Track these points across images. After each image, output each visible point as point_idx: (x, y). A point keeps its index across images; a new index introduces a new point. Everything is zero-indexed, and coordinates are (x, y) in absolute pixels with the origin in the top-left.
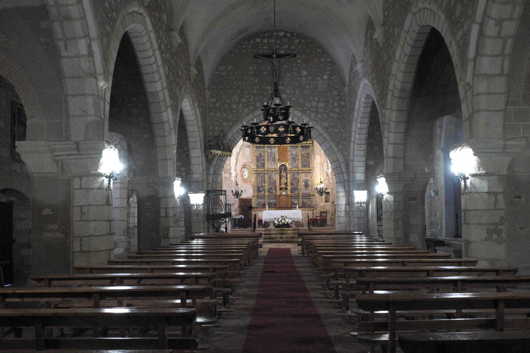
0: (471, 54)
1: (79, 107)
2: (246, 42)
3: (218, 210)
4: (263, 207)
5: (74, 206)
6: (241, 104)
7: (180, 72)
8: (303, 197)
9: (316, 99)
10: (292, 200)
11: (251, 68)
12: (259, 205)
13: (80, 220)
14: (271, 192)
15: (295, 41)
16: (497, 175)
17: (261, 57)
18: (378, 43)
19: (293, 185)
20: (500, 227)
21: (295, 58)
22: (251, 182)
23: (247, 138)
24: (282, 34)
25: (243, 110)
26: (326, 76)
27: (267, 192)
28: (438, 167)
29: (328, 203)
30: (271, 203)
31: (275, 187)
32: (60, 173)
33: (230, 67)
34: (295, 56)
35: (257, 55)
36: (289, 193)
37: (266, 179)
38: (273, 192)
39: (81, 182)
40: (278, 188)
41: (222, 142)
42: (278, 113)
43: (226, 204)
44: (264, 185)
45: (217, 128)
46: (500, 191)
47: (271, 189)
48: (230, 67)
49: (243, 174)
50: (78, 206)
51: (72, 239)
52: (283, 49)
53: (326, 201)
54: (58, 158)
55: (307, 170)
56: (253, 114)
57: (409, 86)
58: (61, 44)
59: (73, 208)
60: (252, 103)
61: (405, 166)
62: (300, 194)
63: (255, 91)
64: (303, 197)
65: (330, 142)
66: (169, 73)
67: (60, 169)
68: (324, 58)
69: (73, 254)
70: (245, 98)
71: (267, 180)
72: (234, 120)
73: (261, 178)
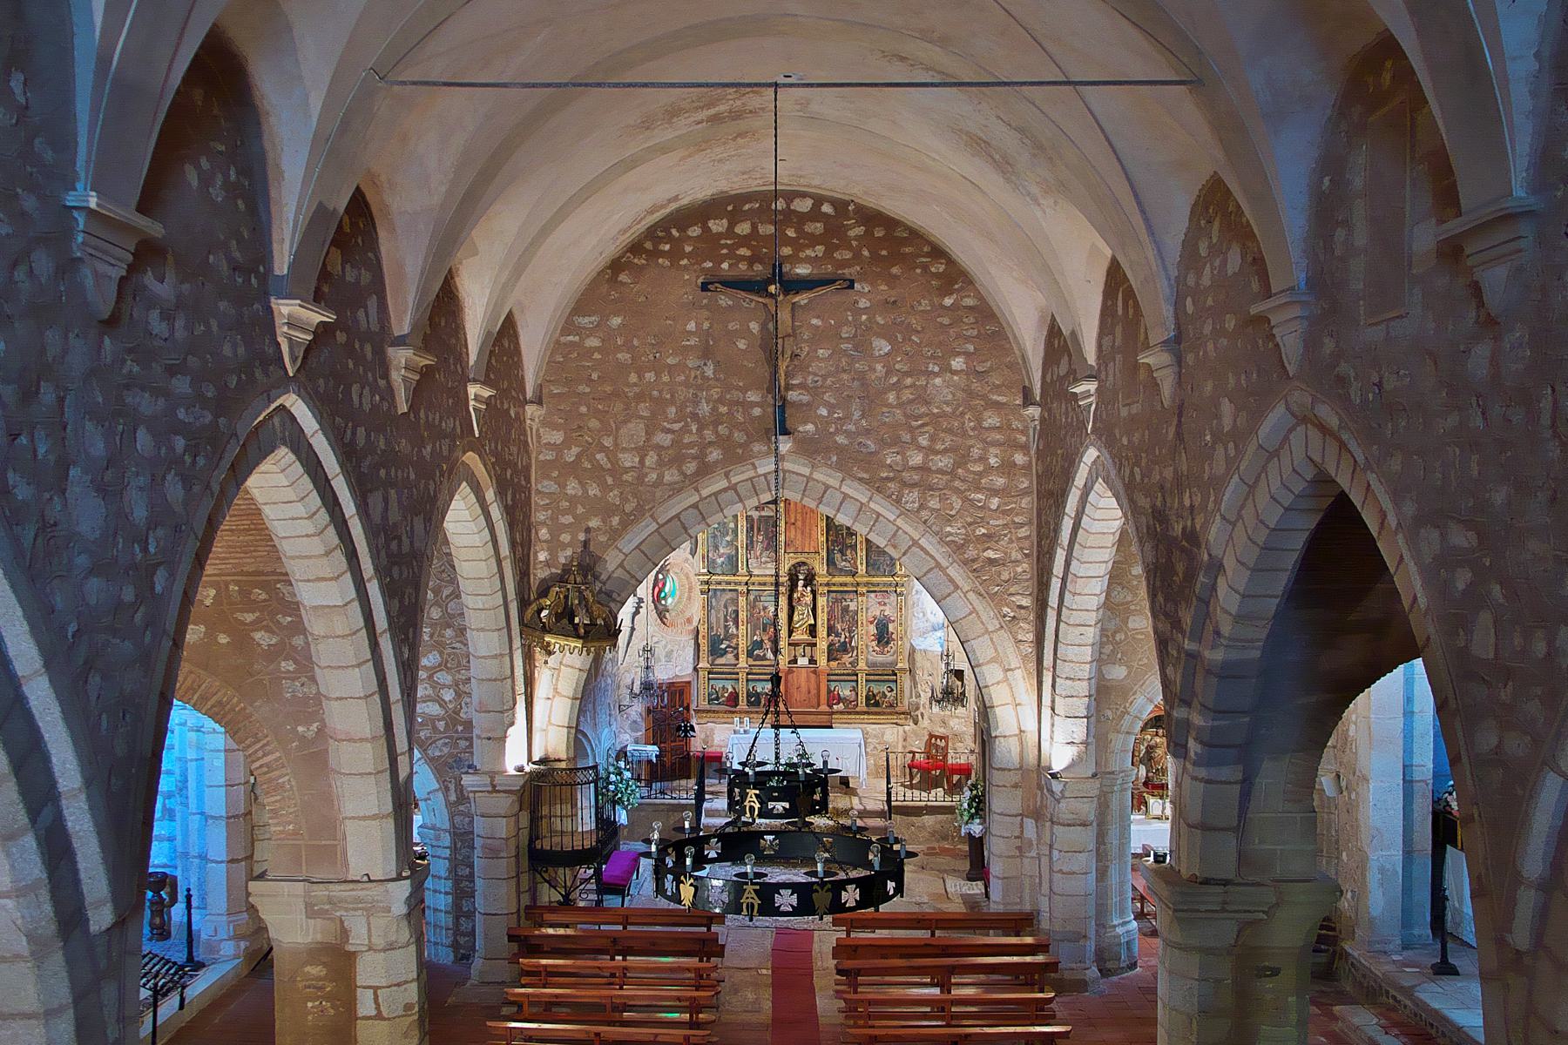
2: (675, 232)
3: (570, 819)
6: (651, 453)
8: (872, 678)
9: (923, 441)
10: (833, 685)
11: (691, 326)
12: (717, 699)
14: (758, 655)
15: (852, 233)
19: (838, 635)
21: (850, 291)
22: (689, 621)
24: (803, 206)
25: (661, 476)
26: (960, 359)
27: (743, 657)
30: (758, 695)
33: (616, 321)
34: (851, 287)
35: (712, 283)
36: (822, 661)
37: (740, 614)
38: (764, 658)
40: (783, 644)
44: (733, 630)
45: (565, 538)
47: (759, 644)
48: (616, 321)
49: (660, 592)
52: (808, 260)
55: (885, 585)
56: (697, 490)
60: (693, 451)
61: (1242, 858)
62: (862, 665)
63: (705, 409)
64: (872, 678)
65: (971, 596)
68: (955, 296)
70: (669, 431)
71: (742, 616)
72: (628, 508)
73: (726, 607)
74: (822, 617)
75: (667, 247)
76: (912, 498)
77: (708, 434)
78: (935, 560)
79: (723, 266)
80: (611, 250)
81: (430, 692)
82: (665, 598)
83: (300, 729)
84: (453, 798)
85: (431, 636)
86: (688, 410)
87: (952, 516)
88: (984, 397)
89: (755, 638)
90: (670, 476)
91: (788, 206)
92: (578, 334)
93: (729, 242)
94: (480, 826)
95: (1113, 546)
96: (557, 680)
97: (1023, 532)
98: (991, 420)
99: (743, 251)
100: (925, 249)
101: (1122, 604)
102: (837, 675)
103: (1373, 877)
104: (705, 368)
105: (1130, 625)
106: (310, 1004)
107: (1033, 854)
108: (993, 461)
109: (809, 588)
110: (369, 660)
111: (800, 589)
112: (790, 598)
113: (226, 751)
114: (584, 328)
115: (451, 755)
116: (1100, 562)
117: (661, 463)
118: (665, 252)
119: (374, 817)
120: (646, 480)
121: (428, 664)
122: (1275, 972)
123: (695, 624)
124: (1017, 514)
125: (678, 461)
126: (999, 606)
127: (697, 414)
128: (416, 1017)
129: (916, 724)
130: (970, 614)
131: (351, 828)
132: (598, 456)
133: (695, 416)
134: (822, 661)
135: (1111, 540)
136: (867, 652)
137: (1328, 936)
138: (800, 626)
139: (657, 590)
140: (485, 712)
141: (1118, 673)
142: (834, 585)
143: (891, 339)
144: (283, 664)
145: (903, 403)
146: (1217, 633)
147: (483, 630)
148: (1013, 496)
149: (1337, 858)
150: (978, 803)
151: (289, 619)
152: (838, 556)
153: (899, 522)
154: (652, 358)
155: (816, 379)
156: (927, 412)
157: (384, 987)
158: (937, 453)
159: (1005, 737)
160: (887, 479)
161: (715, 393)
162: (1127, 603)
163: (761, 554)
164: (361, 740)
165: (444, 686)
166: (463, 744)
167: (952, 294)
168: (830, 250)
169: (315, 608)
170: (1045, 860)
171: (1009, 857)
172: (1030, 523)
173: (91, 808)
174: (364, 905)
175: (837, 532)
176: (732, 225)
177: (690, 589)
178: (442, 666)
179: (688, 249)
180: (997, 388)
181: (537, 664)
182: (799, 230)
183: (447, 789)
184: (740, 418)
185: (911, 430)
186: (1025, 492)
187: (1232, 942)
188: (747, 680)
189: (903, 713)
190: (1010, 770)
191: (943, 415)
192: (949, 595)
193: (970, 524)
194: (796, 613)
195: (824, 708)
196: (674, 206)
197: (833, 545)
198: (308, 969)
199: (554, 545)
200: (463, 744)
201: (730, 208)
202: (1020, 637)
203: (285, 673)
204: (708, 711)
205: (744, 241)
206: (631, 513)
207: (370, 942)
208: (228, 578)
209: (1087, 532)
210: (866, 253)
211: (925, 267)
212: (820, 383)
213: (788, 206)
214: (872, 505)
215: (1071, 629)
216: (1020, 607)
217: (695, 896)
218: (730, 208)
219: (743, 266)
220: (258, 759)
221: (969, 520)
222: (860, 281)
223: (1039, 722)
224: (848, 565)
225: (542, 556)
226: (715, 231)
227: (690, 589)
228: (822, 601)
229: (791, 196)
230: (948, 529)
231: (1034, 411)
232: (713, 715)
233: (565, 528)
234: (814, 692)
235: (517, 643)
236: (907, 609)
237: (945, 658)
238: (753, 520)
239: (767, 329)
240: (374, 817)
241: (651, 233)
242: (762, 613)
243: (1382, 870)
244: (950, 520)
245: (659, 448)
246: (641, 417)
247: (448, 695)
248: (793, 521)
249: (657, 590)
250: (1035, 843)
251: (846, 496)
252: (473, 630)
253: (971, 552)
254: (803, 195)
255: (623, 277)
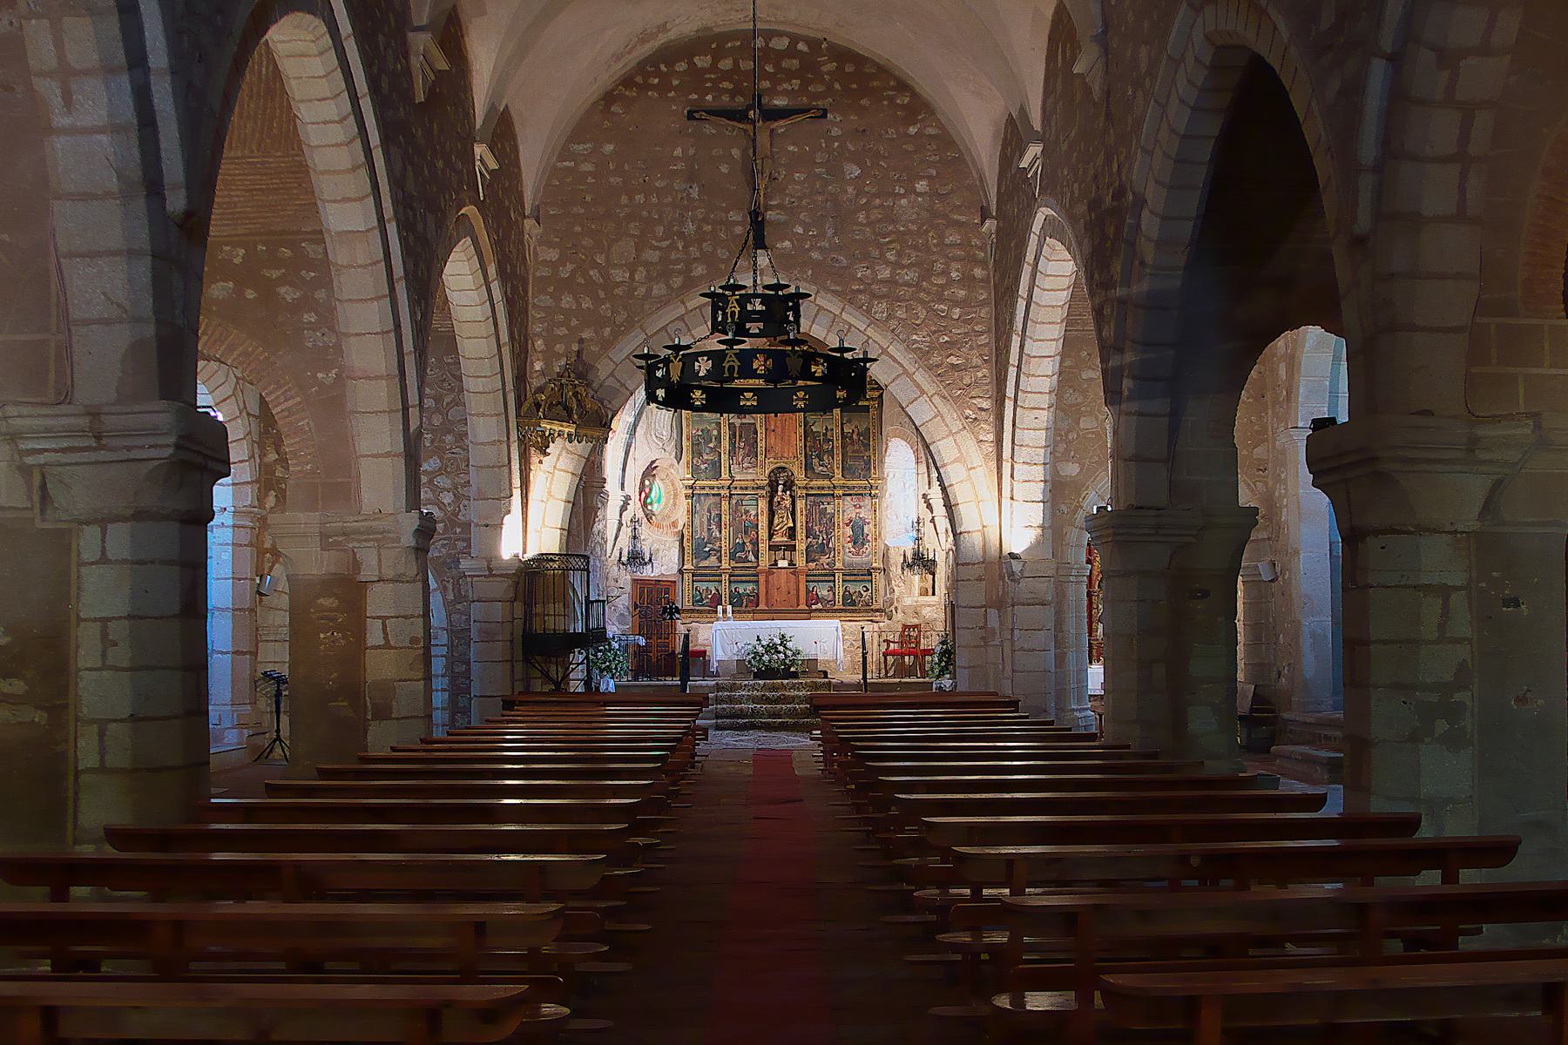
0: (1368, 150)
1: (104, 294)
4: (708, 607)
5: (79, 620)
7: (440, 164)
8: (848, 578)
10: (811, 585)
11: (678, 152)
13: (99, 665)
15: (824, 69)
16: (1449, 533)
17: (712, 118)
18: (1088, 90)
20: (1457, 697)
22: (674, 524)
23: (661, 393)
24: (781, 44)
25: (649, 290)
28: (1283, 487)
29: (930, 599)
31: (755, 543)
32: (37, 511)
34: (824, 116)
35: (697, 112)
36: (800, 561)
37: (723, 516)
38: (746, 560)
39: (103, 541)
40: (763, 546)
41: (576, 394)
42: (731, 368)
43: (589, 602)
46: (1459, 584)
49: (647, 497)
50: (95, 620)
51: (72, 728)
52: (785, 93)
53: (924, 592)
54: (29, 460)
56: (683, 303)
57: (1187, 229)
58: (49, 89)
59: (78, 626)
62: (838, 565)
63: (691, 228)
64: (848, 578)
65: (936, 399)
66: (405, 169)
67: (36, 498)
69: (76, 778)
70: (656, 248)
71: (725, 519)
72: (619, 320)
73: (709, 511)
74: (801, 520)
75: (656, 81)
76: (880, 308)
78: (902, 366)
79: (707, 98)
80: (606, 78)
81: (430, 495)
82: (651, 504)
83: (320, 375)
84: (451, 597)
85: (432, 442)
86: (675, 228)
87: (917, 325)
88: (945, 216)
89: (737, 541)
90: (658, 289)
91: (767, 45)
92: (573, 160)
93: (713, 76)
94: (476, 611)
95: (1062, 321)
96: (551, 483)
97: (983, 339)
98: (953, 237)
99: (726, 85)
100: (892, 84)
101: (1074, 405)
102: (815, 575)
103: (1306, 643)
104: (691, 191)
105: (1082, 426)
107: (997, 642)
108: (954, 275)
109: (788, 492)
110: (385, 296)
111: (780, 493)
112: (771, 503)
113: (233, 544)
114: (579, 154)
115: (449, 555)
116: (1051, 340)
117: (649, 278)
118: (653, 85)
119: (388, 455)
121: (430, 469)
122: (1206, 594)
123: (680, 528)
124: (977, 323)
125: (665, 275)
126: (961, 408)
127: (684, 232)
128: (421, 652)
130: (935, 417)
131: (364, 464)
133: (681, 235)
134: (800, 561)
135: (1060, 314)
136: (845, 555)
137: (1269, 717)
138: (781, 529)
139: (643, 495)
140: (484, 499)
141: (1071, 470)
142: (812, 488)
143: (861, 164)
145: (872, 223)
146: (1142, 263)
147: (483, 415)
148: (972, 307)
149: (1275, 644)
150: (949, 658)
151: (313, 274)
152: (816, 461)
153: (870, 332)
154: (641, 181)
155: (792, 200)
156: (894, 230)
157: (392, 617)
158: (903, 267)
159: (969, 532)
160: (858, 290)
161: (700, 213)
162: (1079, 404)
163: (743, 460)
164: (376, 378)
166: (461, 545)
167: (915, 124)
168: (805, 84)
169: (339, 234)
170: (1007, 644)
171: (975, 647)
172: (989, 331)
173: (174, 92)
174: (375, 536)
175: (815, 438)
176: (716, 60)
177: (675, 495)
178: (442, 471)
179: (675, 82)
180: (957, 209)
181: (532, 468)
182: (777, 66)
183: (445, 588)
185: (880, 246)
186: (983, 303)
188: (730, 582)
189: (877, 611)
190: (974, 564)
191: (909, 232)
192: (916, 399)
193: (934, 333)
195: (803, 607)
196: (662, 39)
197: (810, 450)
198: (321, 601)
199: (549, 355)
200: (461, 545)
201: (713, 46)
202: (981, 437)
203: (307, 323)
204: (692, 611)
205: (726, 76)
206: (622, 325)
207: (380, 572)
208: (257, 238)
209: (1040, 306)
210: (837, 86)
211: (891, 99)
212: (796, 204)
213: (767, 45)
214: (844, 316)
215: (1027, 412)
216: (981, 409)
217: (682, 372)
218: (713, 46)
219: (726, 98)
220: (280, 404)
221: (933, 328)
222: (832, 113)
223: (1000, 516)
224: (825, 469)
225: (538, 366)
226: (700, 66)
227: (675, 495)
228: (800, 504)
229: (769, 35)
230: (915, 337)
231: (990, 225)
232: (697, 615)
233: (559, 339)
234: (793, 592)
235: (514, 436)
236: (881, 512)
237: (916, 524)
238: (735, 427)
239: (748, 155)
240: (388, 455)
241: (641, 67)
242: (744, 517)
243: (1313, 635)
244: (916, 328)
245: (647, 264)
247: (447, 498)
248: (773, 428)
249: (643, 495)
250: (998, 632)
251: (820, 308)
252: (473, 415)
253: (936, 359)
254: (780, 34)
255: (615, 108)
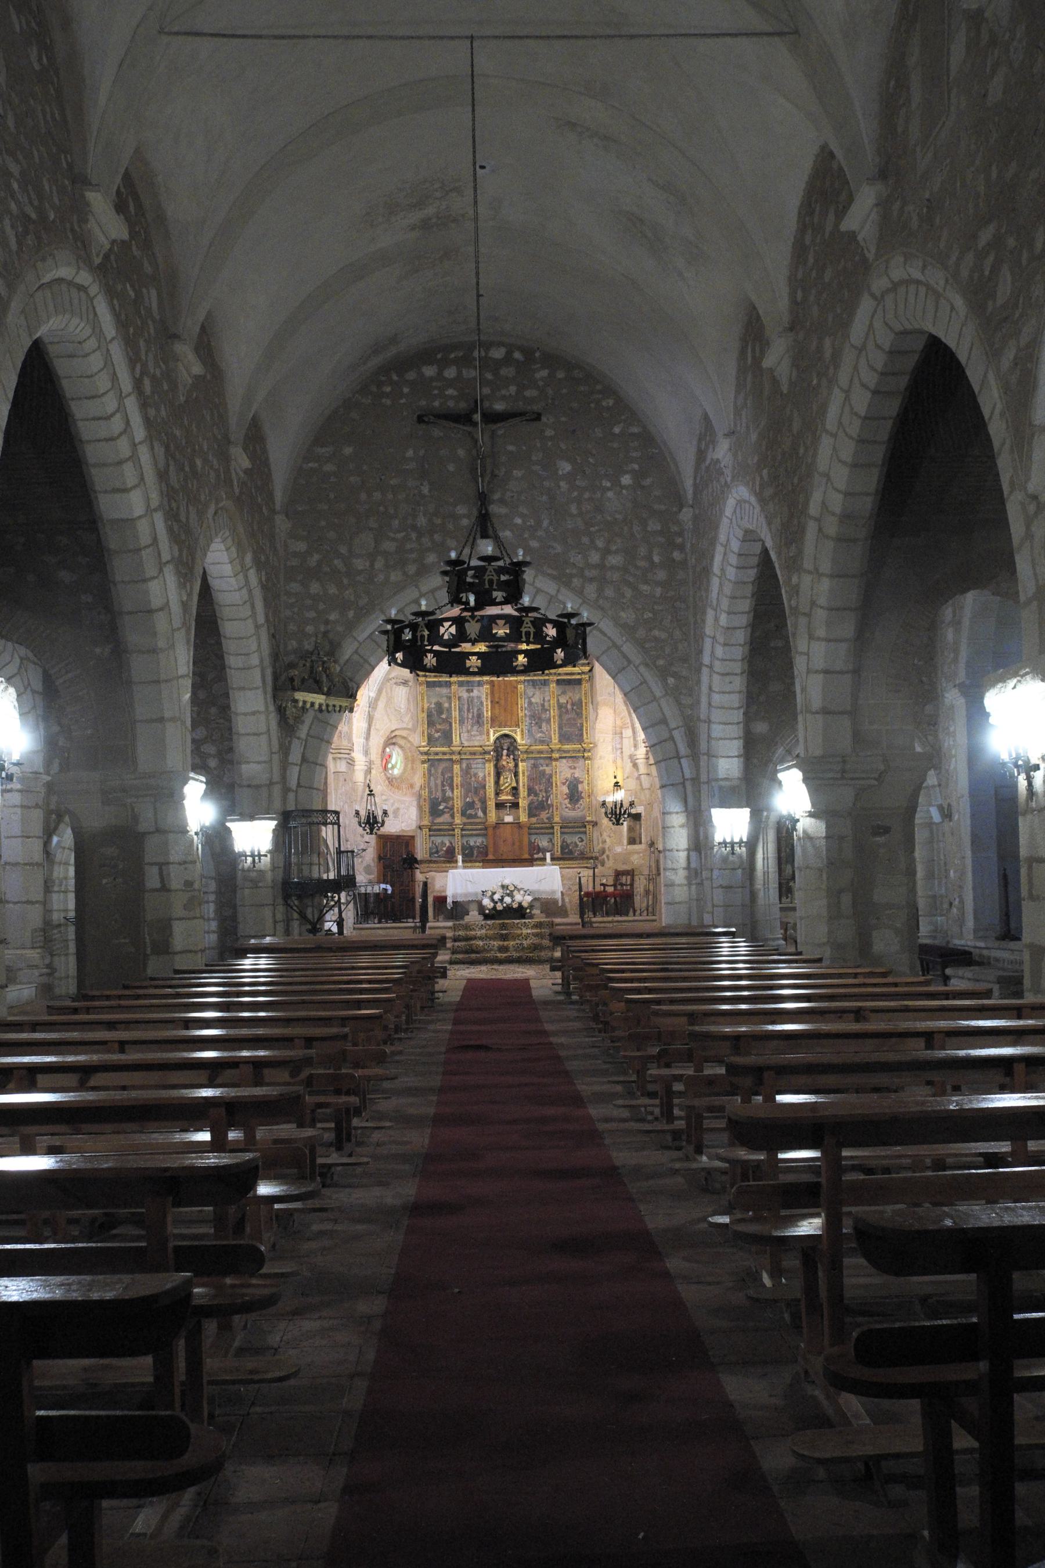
9: (600, 544)
11: (410, 453)
12: (437, 852)
15: (538, 375)
19: (536, 795)
24: (498, 354)
30: (471, 848)
35: (426, 415)
38: (476, 816)
44: (449, 793)
48: (348, 451)
49: (387, 762)
52: (504, 398)
55: (574, 751)
62: (557, 819)
64: (566, 830)
70: (393, 539)
77: (426, 540)
89: (468, 800)
90: (395, 576)
106: (104, 881)
109: (512, 757)
120: (376, 580)
129: (603, 866)
132: (336, 562)
133: (414, 527)
144: (83, 597)
165: (210, 755)
184: (451, 526)
187: (851, 805)
194: (502, 778)
205: (451, 383)
224: (543, 735)
229: (488, 346)
246: (371, 529)
